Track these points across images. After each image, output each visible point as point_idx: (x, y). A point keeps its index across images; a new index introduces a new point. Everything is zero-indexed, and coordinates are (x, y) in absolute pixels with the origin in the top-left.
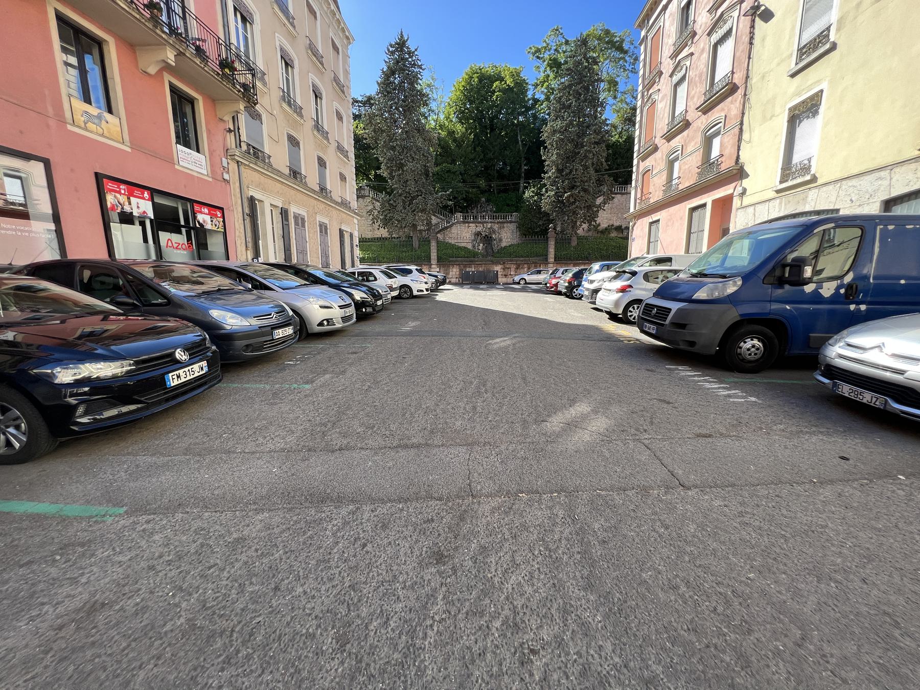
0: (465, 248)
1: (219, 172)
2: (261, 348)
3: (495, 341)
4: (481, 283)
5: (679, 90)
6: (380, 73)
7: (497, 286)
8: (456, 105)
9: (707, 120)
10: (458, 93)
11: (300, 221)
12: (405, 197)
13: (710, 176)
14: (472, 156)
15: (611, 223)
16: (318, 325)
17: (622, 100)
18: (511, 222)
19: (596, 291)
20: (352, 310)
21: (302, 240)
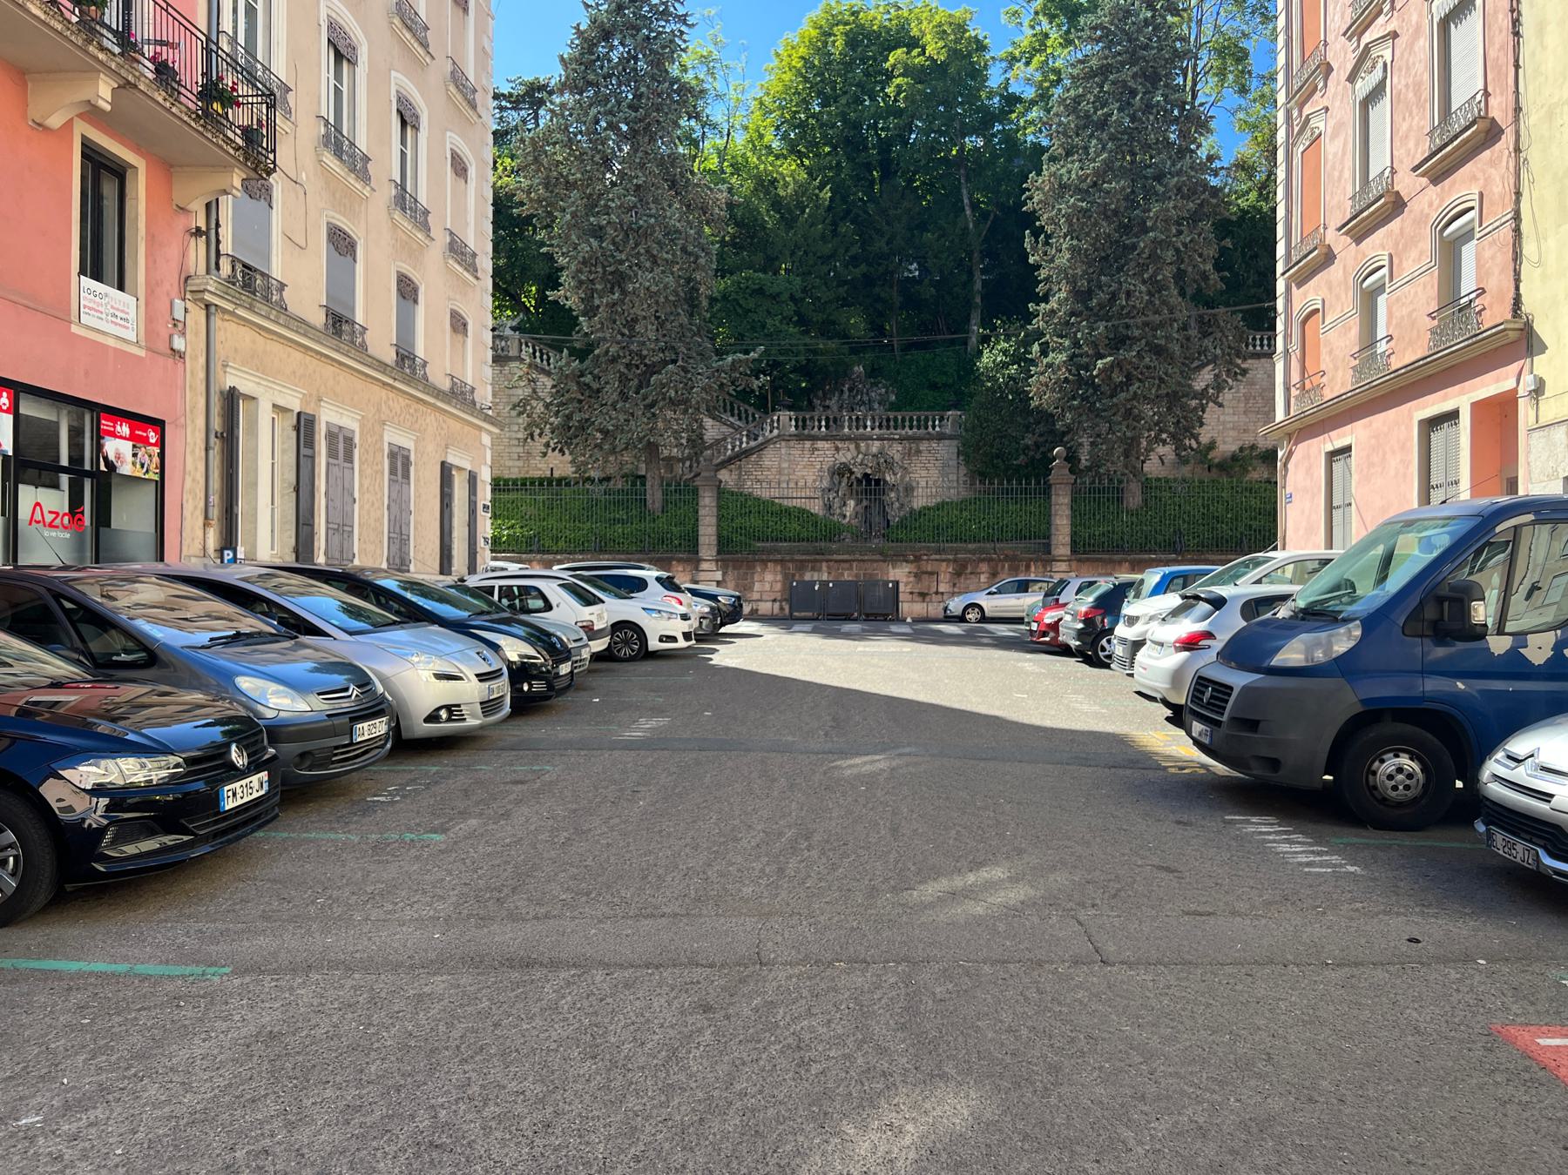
0: (802, 511)
1: (164, 334)
2: (326, 762)
3: (852, 762)
4: (848, 618)
5: (1374, 114)
6: (571, 35)
7: (894, 628)
8: (782, 108)
9: (1442, 200)
10: (787, 77)
11: (341, 446)
12: (628, 366)
13: (1458, 342)
14: (827, 249)
15: (1248, 439)
16: (428, 720)
17: (1263, 96)
18: (941, 437)
19: (1137, 645)
20: (502, 687)
21: (343, 496)
